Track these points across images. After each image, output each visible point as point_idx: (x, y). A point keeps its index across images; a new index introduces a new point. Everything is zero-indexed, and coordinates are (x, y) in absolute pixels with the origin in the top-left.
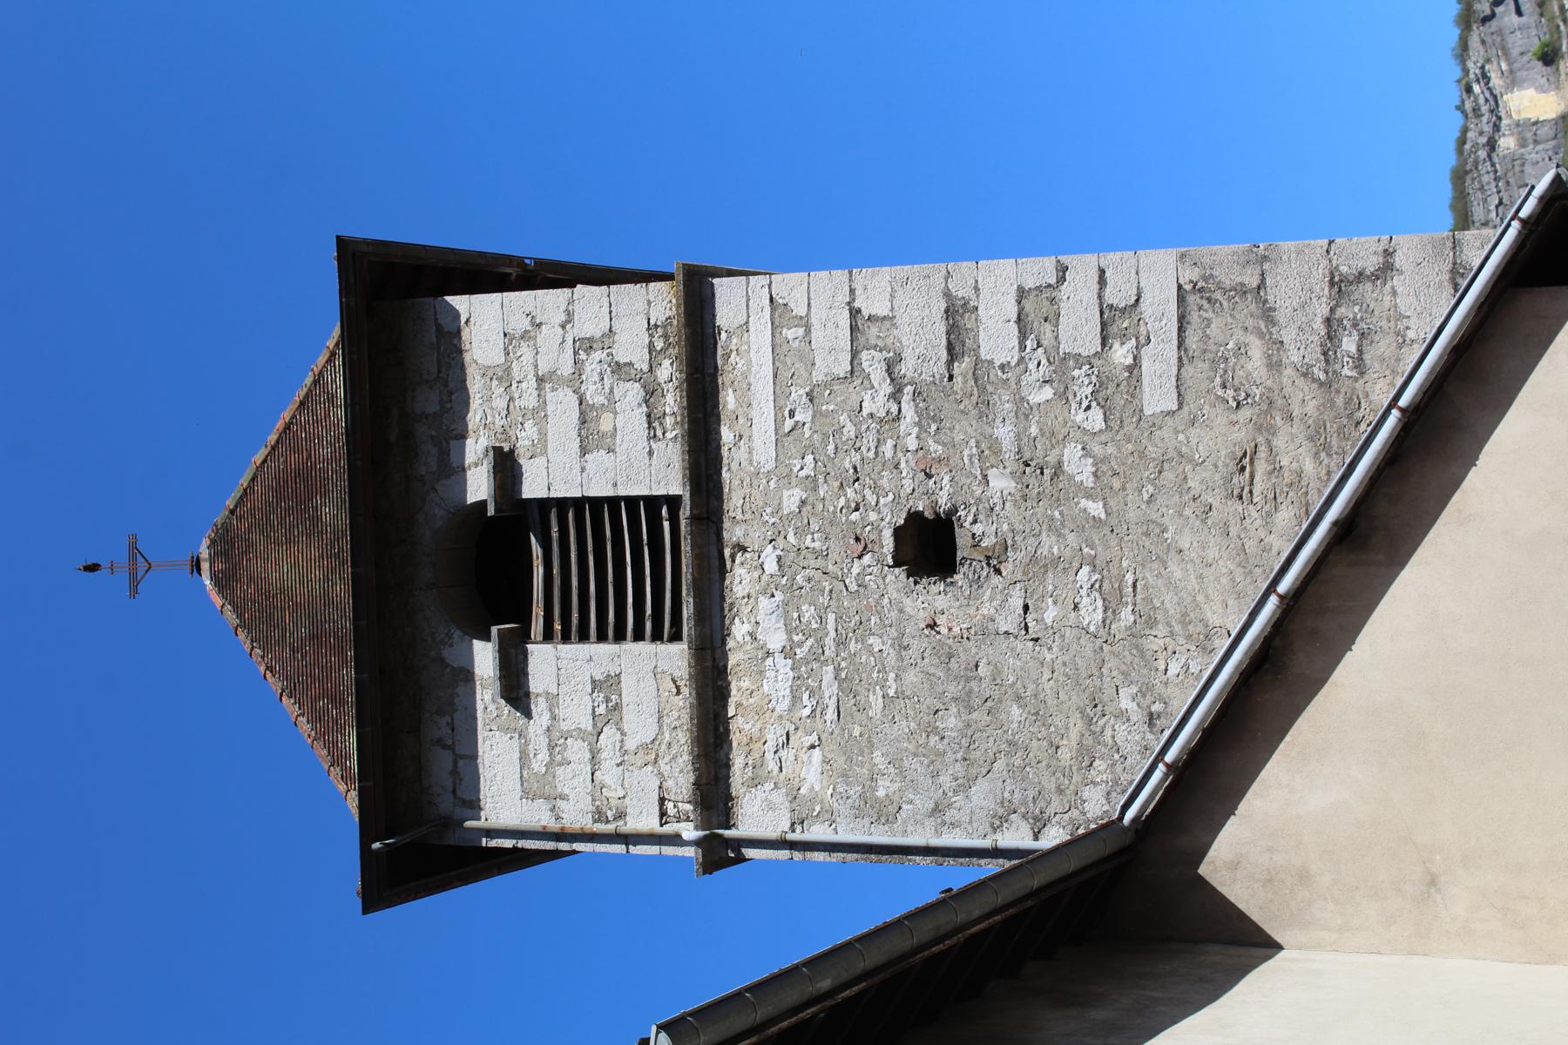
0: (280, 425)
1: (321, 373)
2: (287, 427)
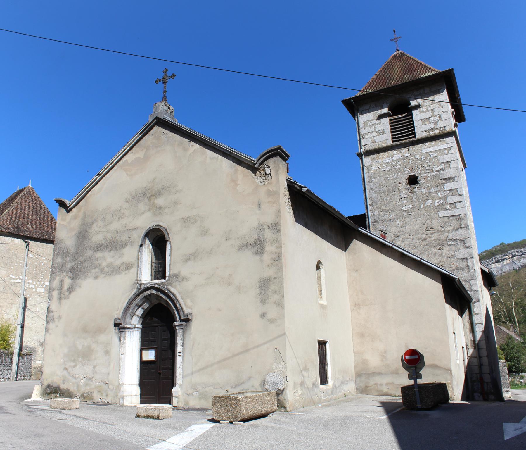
2: (421, 64)
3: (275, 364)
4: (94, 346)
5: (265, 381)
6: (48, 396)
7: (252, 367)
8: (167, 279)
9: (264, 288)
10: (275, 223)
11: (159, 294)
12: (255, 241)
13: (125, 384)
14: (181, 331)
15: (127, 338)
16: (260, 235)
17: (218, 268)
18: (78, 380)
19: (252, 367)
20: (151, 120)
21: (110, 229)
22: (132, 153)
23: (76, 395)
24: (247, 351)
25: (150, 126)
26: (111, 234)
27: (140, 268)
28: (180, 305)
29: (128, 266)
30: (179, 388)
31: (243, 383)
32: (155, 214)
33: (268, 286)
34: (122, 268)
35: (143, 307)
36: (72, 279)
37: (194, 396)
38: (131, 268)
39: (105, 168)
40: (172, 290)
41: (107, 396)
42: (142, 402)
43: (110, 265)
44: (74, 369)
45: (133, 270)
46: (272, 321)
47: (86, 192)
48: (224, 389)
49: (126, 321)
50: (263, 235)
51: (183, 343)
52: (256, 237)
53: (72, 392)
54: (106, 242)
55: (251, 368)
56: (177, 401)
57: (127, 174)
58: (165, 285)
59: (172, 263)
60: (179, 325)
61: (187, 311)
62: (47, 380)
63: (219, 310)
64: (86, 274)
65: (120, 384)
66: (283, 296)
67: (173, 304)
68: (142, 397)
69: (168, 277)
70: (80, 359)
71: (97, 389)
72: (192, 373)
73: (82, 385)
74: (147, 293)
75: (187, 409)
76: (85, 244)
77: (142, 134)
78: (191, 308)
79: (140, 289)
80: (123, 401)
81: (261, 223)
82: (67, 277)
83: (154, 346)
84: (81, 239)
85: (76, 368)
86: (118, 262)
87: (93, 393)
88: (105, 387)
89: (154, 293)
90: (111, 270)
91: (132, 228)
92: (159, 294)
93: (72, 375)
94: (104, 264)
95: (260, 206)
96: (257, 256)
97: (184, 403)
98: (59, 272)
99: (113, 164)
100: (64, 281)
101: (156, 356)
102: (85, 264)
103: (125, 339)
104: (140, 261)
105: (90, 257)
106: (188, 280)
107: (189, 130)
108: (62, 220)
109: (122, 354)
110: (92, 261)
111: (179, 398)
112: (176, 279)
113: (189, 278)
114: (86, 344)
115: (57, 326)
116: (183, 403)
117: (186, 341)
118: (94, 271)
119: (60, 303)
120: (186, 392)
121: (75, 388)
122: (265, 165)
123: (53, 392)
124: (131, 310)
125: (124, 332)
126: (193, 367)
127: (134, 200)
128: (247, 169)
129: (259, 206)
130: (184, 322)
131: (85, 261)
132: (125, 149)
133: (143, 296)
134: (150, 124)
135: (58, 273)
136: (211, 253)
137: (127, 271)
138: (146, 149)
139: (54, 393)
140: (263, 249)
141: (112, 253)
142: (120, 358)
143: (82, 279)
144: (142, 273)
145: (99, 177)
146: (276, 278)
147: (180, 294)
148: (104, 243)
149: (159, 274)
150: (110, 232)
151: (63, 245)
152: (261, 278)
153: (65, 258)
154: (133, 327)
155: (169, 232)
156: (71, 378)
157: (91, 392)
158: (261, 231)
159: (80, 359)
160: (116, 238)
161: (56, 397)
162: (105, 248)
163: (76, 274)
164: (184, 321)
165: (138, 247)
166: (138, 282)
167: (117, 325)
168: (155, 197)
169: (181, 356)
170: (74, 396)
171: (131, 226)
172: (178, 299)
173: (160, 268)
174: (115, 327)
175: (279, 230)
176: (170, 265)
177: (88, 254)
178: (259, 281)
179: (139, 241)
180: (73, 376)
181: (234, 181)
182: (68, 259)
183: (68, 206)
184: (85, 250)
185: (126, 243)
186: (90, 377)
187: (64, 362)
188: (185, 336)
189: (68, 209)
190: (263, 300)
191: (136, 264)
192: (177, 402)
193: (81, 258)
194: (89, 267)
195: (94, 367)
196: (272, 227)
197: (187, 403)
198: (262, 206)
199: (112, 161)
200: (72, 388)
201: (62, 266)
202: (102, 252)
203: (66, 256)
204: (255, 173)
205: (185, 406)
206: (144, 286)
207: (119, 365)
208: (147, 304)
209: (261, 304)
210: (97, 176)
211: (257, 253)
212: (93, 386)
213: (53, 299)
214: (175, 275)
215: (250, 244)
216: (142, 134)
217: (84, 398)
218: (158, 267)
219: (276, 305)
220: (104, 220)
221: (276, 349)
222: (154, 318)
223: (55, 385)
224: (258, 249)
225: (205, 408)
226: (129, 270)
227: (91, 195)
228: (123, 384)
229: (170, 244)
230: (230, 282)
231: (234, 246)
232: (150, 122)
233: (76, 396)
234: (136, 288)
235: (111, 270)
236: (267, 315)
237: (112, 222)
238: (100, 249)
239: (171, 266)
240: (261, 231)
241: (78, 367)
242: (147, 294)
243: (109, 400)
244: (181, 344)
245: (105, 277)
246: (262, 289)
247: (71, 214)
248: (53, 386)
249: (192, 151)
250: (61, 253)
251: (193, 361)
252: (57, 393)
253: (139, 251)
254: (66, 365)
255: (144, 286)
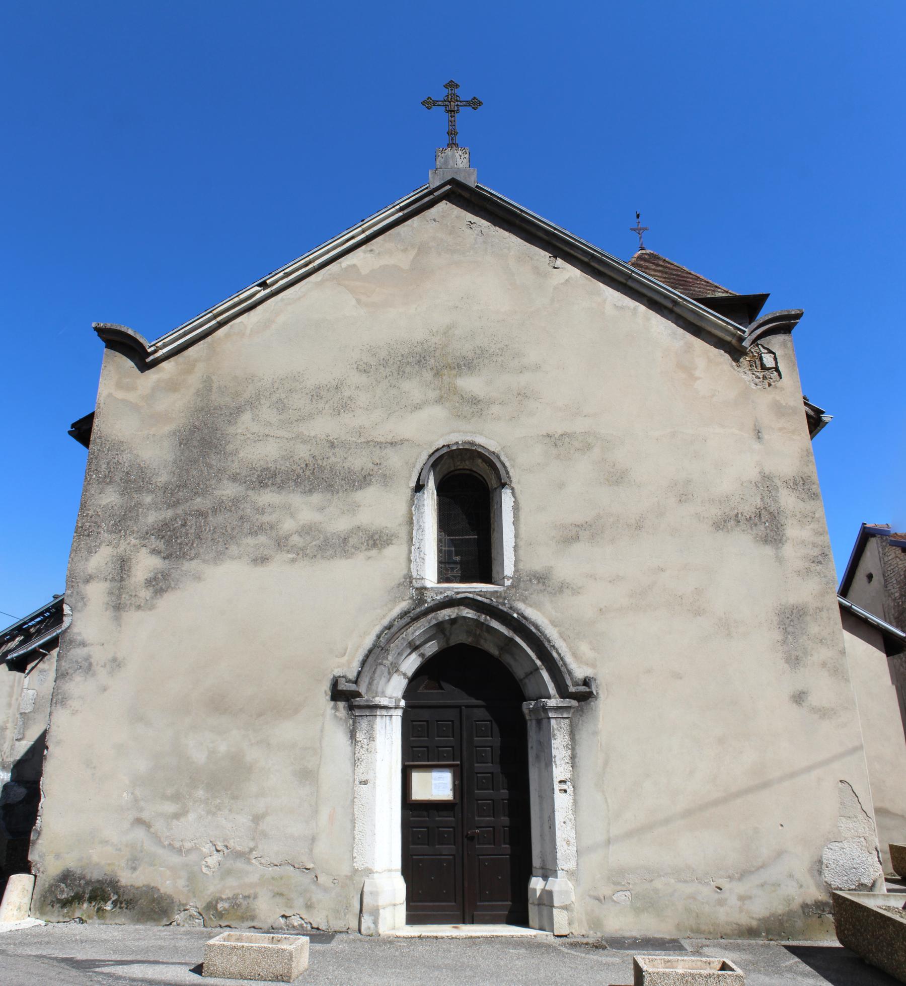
0: (698, 275)
1: (720, 288)
2: (698, 278)
3: (844, 820)
4: (253, 754)
5: (820, 862)
6: (65, 911)
7: (782, 825)
8: (508, 583)
9: (790, 629)
10: (802, 478)
11: (486, 620)
12: (758, 512)
13: (375, 871)
14: (565, 724)
15: (378, 736)
16: (767, 500)
17: (662, 570)
18: (193, 857)
19: (782, 825)
20: (437, 184)
21: (305, 433)
22: (371, 251)
23: (186, 905)
24: (765, 785)
25: (432, 197)
26: (309, 447)
27: (417, 545)
28: (559, 654)
29: (376, 537)
30: (569, 882)
31: (762, 867)
32: (460, 413)
33: (803, 625)
34: (353, 541)
35: (422, 651)
36: (164, 558)
37: (618, 903)
38: (388, 545)
39: (286, 271)
40: (531, 613)
41: (309, 907)
42: (412, 920)
43: (307, 530)
44: (175, 822)
45: (395, 552)
46: (824, 713)
47: (214, 322)
48: (707, 884)
49: (374, 687)
50: (776, 501)
51: (573, 757)
52: (759, 503)
53: (170, 896)
54: (294, 467)
55: (780, 828)
56: (567, 918)
57: (359, 301)
58: (505, 599)
59: (521, 543)
60: (557, 709)
61: (580, 672)
62: (58, 856)
63: (678, 676)
64: (221, 547)
65: (356, 870)
66: (845, 653)
67: (533, 651)
68: (411, 904)
69: (511, 578)
70: (200, 793)
71: (271, 888)
72: (608, 842)
73: (208, 872)
74: (446, 614)
75: (598, 946)
76: (214, 463)
77: (405, 212)
78: (594, 666)
79: (421, 601)
80: (376, 923)
81: (767, 473)
82: (144, 550)
83: (445, 759)
84: (195, 447)
85: (183, 820)
86: (341, 525)
87: (255, 897)
88: (305, 880)
89: (469, 616)
90: (314, 543)
91: (382, 439)
92: (486, 620)
93: (166, 843)
94: (288, 525)
95: (759, 434)
96: (767, 547)
97: (588, 924)
98: (111, 532)
99: (311, 266)
100: (134, 561)
101: (459, 787)
102: (219, 519)
103: (372, 738)
104: (415, 528)
105: (236, 501)
106: (576, 591)
107: (555, 229)
108: (119, 386)
109: (365, 782)
110: (240, 513)
111: (572, 911)
112: (540, 586)
113: (580, 588)
114: (223, 748)
115: (105, 690)
116: (586, 924)
117: (582, 752)
118: (250, 541)
119: (117, 619)
120: (592, 893)
121: (181, 883)
122: (760, 346)
123: (87, 896)
124: (390, 658)
125: (371, 717)
126: (609, 824)
127: (387, 369)
128: (716, 347)
129: (758, 434)
130: (576, 702)
131: (215, 511)
132: (352, 238)
133: (434, 622)
134: (431, 193)
135: (105, 536)
136: (639, 527)
137: (374, 552)
138: (416, 250)
139: (90, 900)
140: (781, 534)
141: (316, 498)
142: (354, 792)
143: (204, 561)
144: (423, 559)
145: (263, 293)
146: (821, 610)
147: (555, 626)
148: (283, 468)
149: (452, 569)
150: (304, 442)
151: (125, 458)
152: (780, 604)
153: (135, 495)
154: (392, 705)
155: (507, 464)
156: (160, 851)
157: (246, 897)
158: (770, 492)
159: (200, 793)
160: (330, 461)
161: (97, 912)
162: (292, 483)
163: (181, 544)
164: (574, 699)
165: (408, 492)
166: (411, 582)
167: (337, 694)
168: (454, 372)
169: (568, 791)
170: (176, 908)
171: (383, 433)
172: (550, 639)
173: (456, 555)
174: (333, 703)
175: (814, 494)
176: (516, 548)
177: (224, 493)
178: (777, 612)
179: (411, 476)
180: (170, 844)
181: (687, 369)
182: (148, 499)
183: (149, 350)
184: (213, 482)
185: (365, 477)
186: (238, 848)
187: (136, 800)
188: (577, 737)
189: (148, 360)
190: (793, 658)
191: (403, 533)
192: (567, 922)
193: (199, 500)
194: (233, 529)
195: (257, 819)
196: (797, 485)
197: (596, 923)
198: (766, 436)
199: (311, 257)
200: (168, 882)
201: (124, 518)
202: (279, 493)
203: (139, 490)
204: (736, 360)
205: (591, 932)
206: (433, 594)
207: (354, 815)
208: (436, 644)
209: (786, 666)
210: (259, 288)
211: (766, 540)
212: (254, 878)
213: (85, 604)
214: (535, 576)
215: (743, 518)
216: (405, 212)
217: (220, 915)
218: (450, 552)
219: (829, 671)
220: (281, 407)
221: (841, 781)
222: (444, 684)
223: (95, 875)
224: (768, 531)
225: (656, 936)
226: (380, 549)
227: (228, 335)
228: (369, 872)
229: (513, 494)
230: (699, 608)
231: (704, 517)
232: (432, 187)
233: (187, 910)
234: (407, 598)
235: (314, 543)
236: (809, 698)
237: (311, 417)
238: (273, 484)
239: (521, 552)
240: (770, 492)
241: (191, 817)
242: (447, 618)
243: (318, 919)
244: (568, 760)
245: (293, 561)
246: (786, 632)
247: (153, 375)
248: (88, 877)
249: (563, 281)
250: (117, 478)
251: (608, 806)
252: (105, 899)
253: (412, 502)
254: (141, 810)
255: (433, 594)
